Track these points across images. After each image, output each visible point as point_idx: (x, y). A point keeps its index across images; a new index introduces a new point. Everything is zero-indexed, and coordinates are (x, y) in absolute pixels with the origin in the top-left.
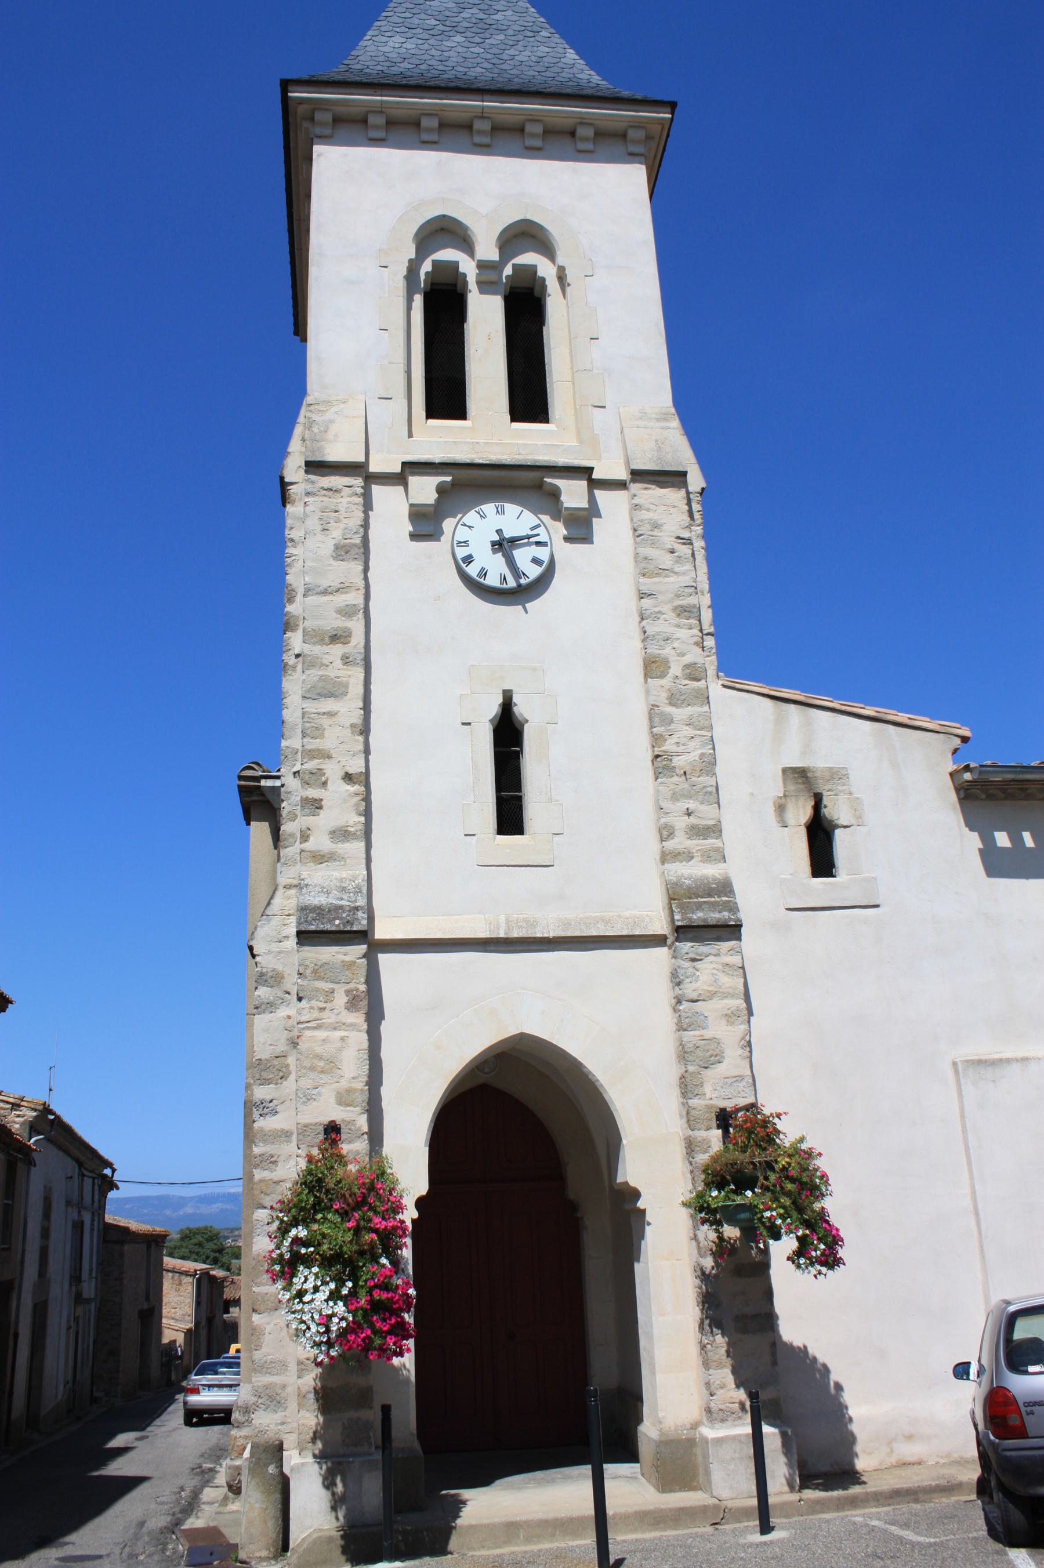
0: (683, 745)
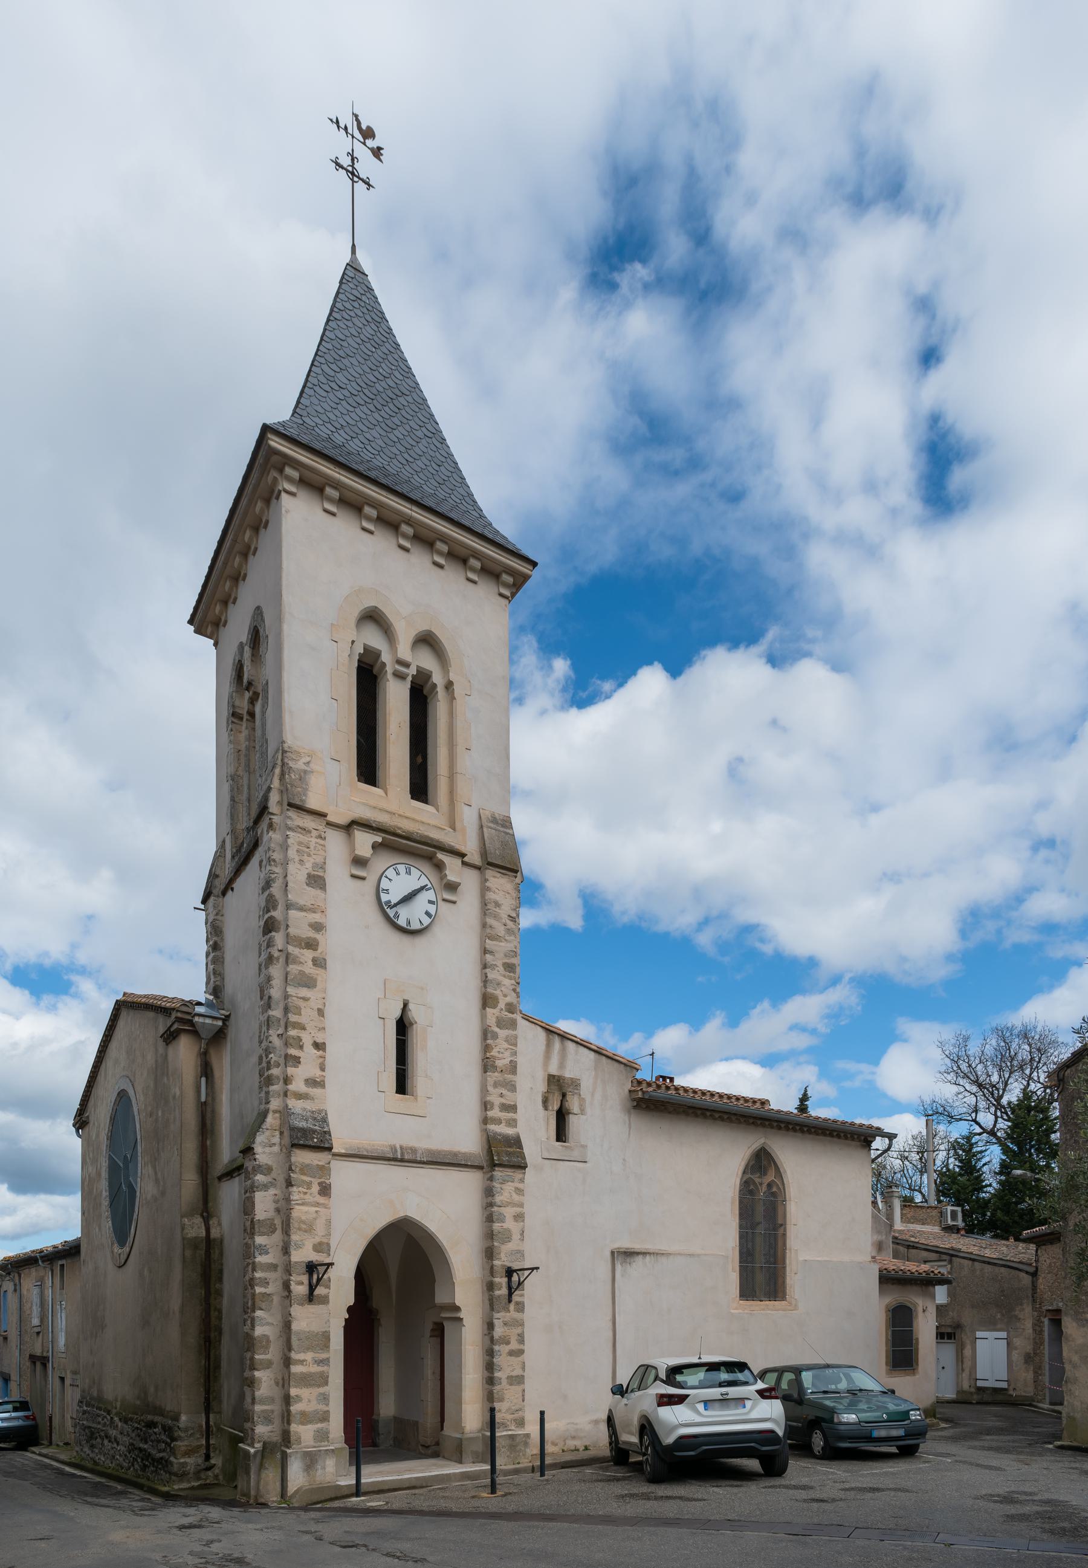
0: (502, 1053)
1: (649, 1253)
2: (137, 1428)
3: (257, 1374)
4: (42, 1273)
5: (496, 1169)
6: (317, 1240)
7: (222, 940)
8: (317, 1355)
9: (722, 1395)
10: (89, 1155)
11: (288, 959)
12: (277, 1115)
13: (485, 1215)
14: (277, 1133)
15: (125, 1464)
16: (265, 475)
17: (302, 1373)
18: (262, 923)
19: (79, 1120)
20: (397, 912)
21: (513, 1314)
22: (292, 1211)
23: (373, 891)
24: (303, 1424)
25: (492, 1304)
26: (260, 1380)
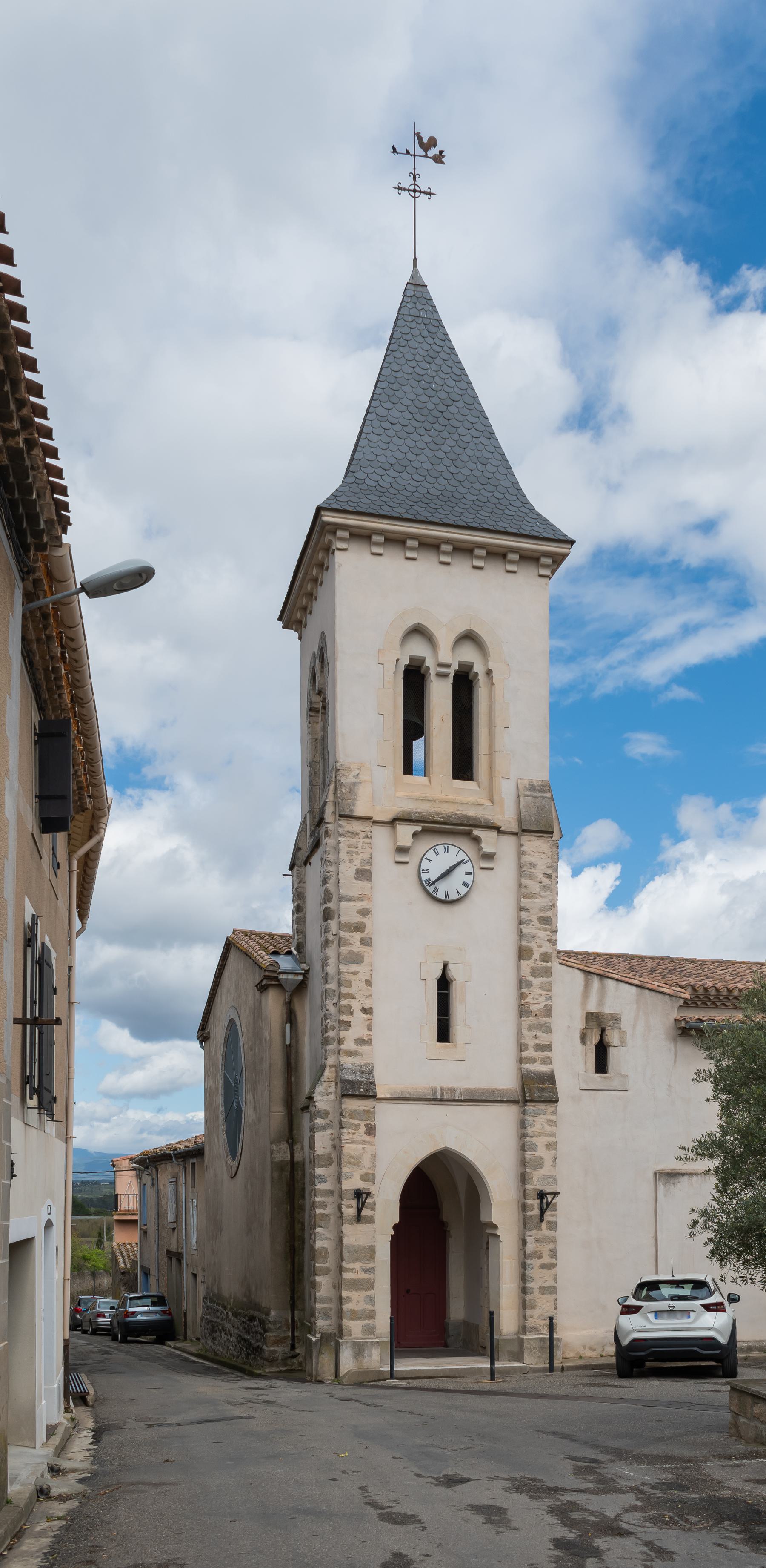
0: (536, 999)
1: (695, 1174)
2: (243, 1322)
3: (318, 1278)
4: (176, 1169)
5: (528, 1104)
6: (364, 1171)
7: (304, 902)
8: (364, 1265)
9: (669, 1307)
11: (341, 942)
12: (333, 1069)
13: (521, 1145)
14: (333, 1084)
15: (236, 1354)
16: (323, 536)
17: (352, 1279)
18: (322, 910)
19: (201, 1035)
20: (436, 888)
21: (544, 1231)
22: (343, 1149)
24: (352, 1320)
25: (525, 1223)
26: (320, 1284)
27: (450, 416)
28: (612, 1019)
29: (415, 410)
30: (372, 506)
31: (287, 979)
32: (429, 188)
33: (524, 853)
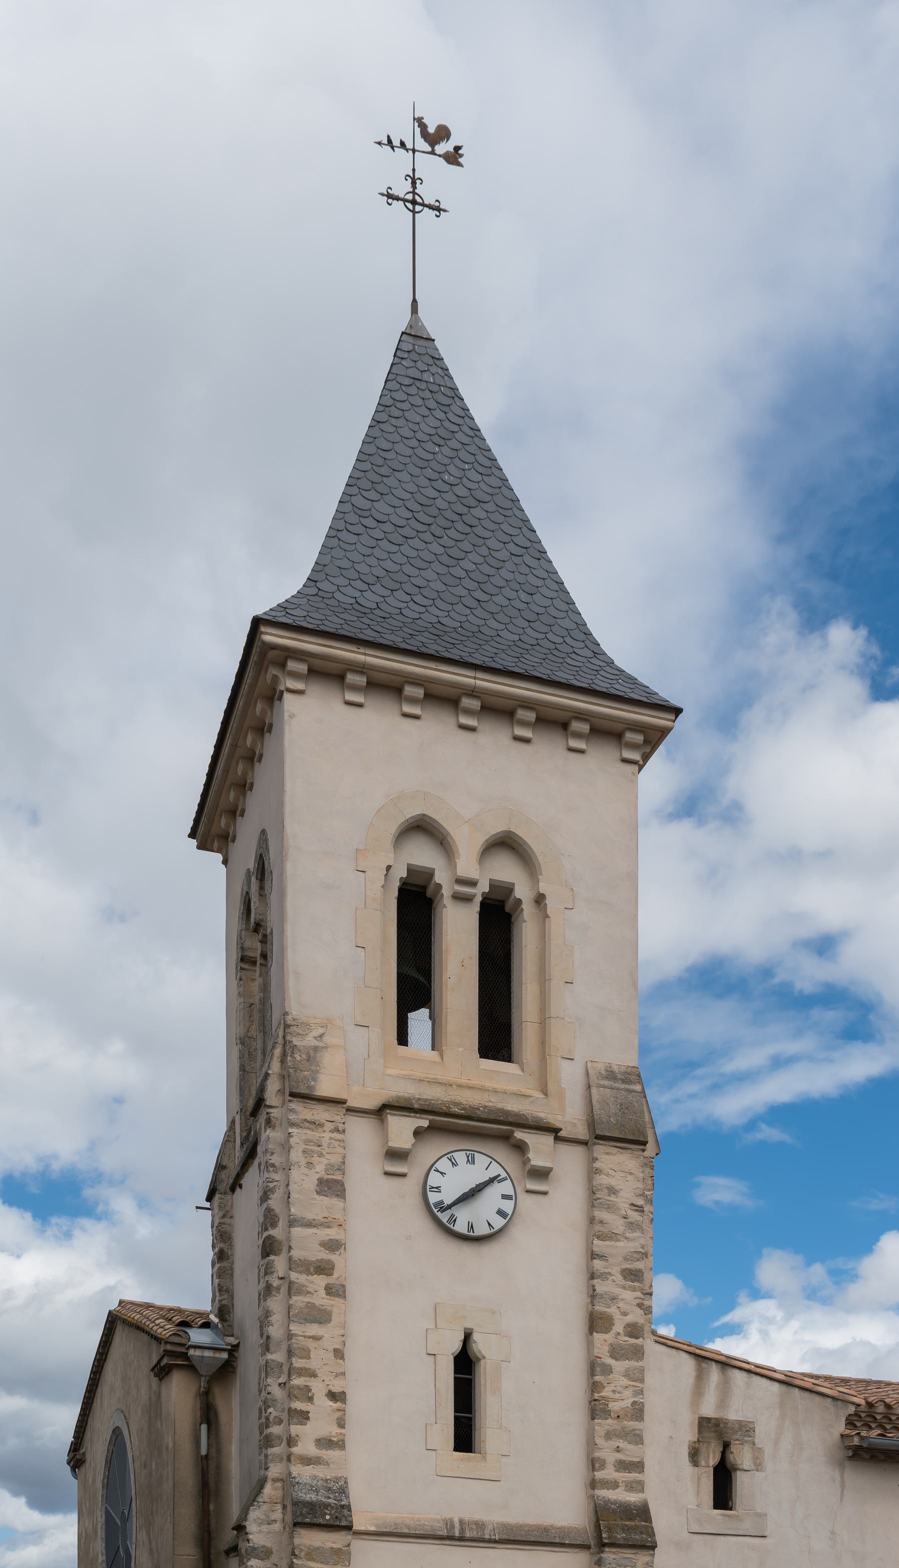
0: (619, 1393)
5: (607, 1549)
7: (231, 1246)
10: (85, 1504)
11: (292, 1289)
12: (279, 1484)
14: (279, 1507)
16: (262, 672)
18: (261, 1242)
20: (452, 1215)
23: (418, 1189)
27: (475, 522)
28: (740, 1429)
29: (416, 507)
30: (345, 626)
31: (202, 1357)
32: (437, 201)
33: (598, 1171)
